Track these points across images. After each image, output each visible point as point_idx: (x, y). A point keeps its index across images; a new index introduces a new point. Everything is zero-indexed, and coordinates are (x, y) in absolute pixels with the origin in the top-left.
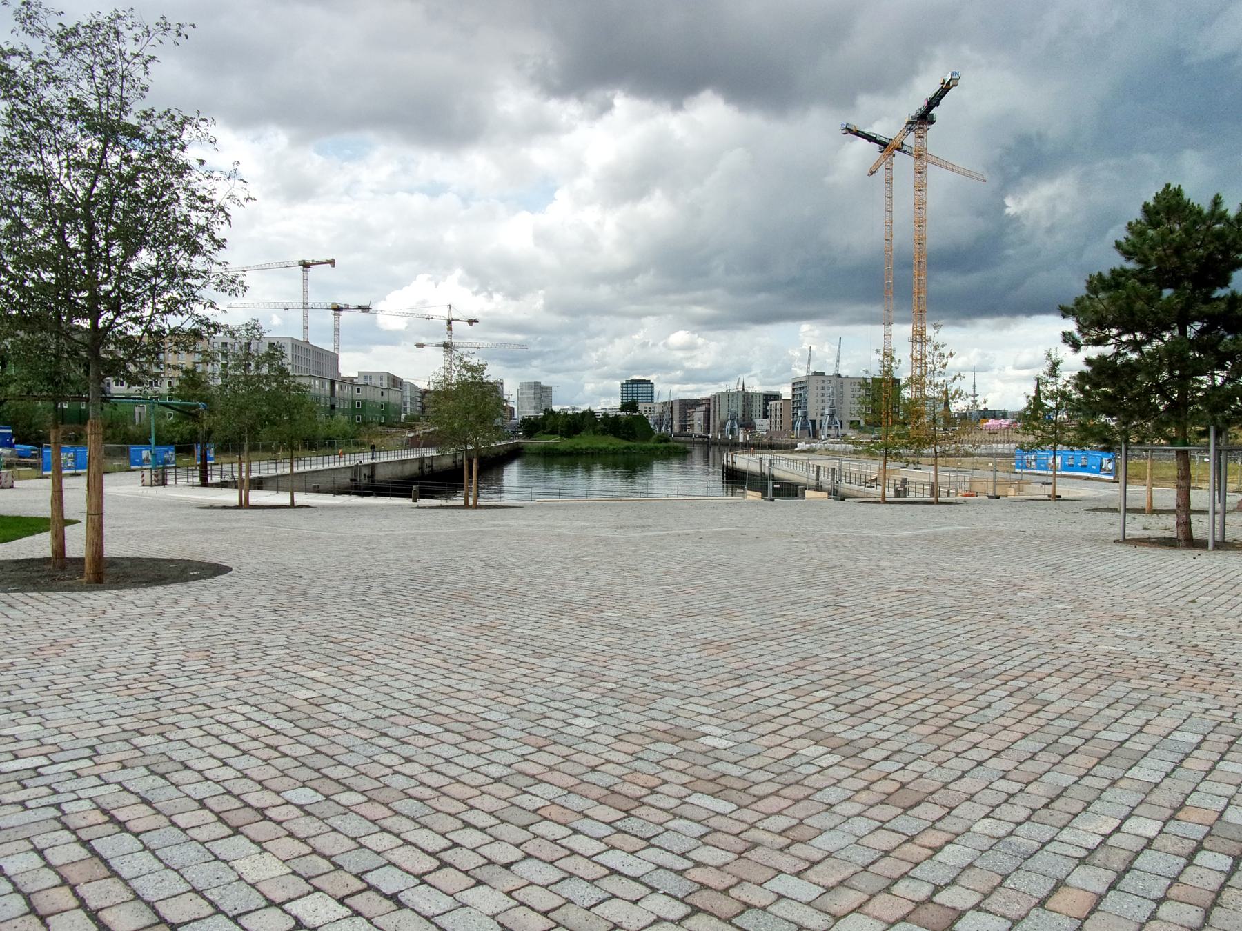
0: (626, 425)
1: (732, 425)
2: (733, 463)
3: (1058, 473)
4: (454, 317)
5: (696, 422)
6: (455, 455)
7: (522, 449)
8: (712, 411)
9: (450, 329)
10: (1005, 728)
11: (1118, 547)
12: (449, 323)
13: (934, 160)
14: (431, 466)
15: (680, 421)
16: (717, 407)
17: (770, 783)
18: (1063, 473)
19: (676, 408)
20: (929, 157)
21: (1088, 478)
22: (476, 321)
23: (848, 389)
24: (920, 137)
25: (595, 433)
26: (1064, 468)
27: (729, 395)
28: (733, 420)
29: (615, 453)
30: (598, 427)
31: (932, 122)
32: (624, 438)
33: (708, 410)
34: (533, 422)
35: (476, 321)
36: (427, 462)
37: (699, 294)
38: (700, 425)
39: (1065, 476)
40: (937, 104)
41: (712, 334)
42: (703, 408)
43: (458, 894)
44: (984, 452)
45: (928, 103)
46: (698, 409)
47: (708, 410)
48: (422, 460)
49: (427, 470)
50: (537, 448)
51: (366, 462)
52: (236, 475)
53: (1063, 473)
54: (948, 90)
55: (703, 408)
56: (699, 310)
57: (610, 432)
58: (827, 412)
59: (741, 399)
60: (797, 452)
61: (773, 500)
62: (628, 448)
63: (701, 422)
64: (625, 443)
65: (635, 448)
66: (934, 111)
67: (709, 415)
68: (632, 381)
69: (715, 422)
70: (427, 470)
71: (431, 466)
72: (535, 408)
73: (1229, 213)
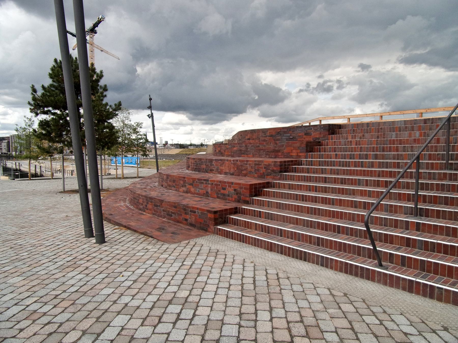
2: (6, 165)
3: (124, 165)
5: (3, 147)
8: (11, 142)
10: (118, 254)
11: (63, 195)
13: (97, 46)
17: (4, 294)
18: (126, 165)
20: (95, 45)
21: (133, 167)
24: (91, 38)
26: (128, 163)
31: (96, 33)
33: (9, 142)
37: (7, 91)
38: (5, 148)
39: (126, 166)
40: (97, 26)
41: (13, 109)
42: (6, 141)
43: (340, 330)
45: (94, 25)
46: (4, 141)
47: (9, 142)
52: (103, 157)
53: (126, 165)
54: (101, 22)
55: (6, 141)
56: (6, 98)
61: (14, 179)
63: (6, 147)
66: (96, 29)
67: (9, 144)
73: (46, 85)
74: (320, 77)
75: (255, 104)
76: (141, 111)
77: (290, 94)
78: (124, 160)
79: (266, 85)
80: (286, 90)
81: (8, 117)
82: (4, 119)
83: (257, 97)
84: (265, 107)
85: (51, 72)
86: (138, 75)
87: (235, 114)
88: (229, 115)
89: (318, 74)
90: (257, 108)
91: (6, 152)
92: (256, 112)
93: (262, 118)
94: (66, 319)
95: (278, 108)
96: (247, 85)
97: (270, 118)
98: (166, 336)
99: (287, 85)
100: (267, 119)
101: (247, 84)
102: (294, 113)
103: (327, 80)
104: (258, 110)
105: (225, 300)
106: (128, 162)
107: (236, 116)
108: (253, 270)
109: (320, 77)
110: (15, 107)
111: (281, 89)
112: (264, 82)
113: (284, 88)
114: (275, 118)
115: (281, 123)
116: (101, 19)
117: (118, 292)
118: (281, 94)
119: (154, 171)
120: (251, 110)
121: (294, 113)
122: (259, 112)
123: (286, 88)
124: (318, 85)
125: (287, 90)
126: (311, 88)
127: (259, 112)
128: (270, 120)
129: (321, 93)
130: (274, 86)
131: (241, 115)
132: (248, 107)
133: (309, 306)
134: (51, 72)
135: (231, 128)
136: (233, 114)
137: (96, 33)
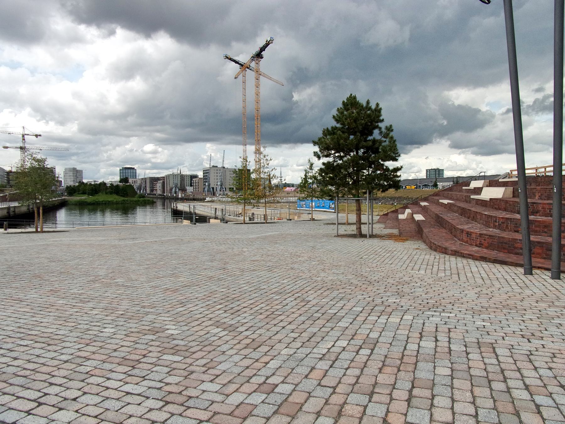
0: (122, 190)
1: (175, 190)
3: (313, 209)
4: (26, 133)
6: (29, 206)
7: (67, 202)
8: (165, 183)
9: (24, 139)
12: (23, 136)
14: (14, 211)
15: (150, 188)
16: (168, 181)
18: (316, 209)
19: (148, 181)
21: (325, 211)
22: (40, 136)
23: (228, 173)
25: (106, 193)
26: (318, 207)
27: (174, 175)
28: (176, 187)
29: (117, 203)
30: (108, 191)
31: (262, 58)
32: (121, 196)
33: (164, 182)
34: (73, 188)
35: (40, 136)
36: (12, 209)
37: (159, 127)
39: (316, 211)
40: (264, 50)
42: (161, 181)
44: (285, 201)
46: (159, 182)
47: (164, 182)
48: (9, 208)
49: (12, 213)
50: (75, 201)
51: (12, 206)
53: (316, 209)
54: (269, 44)
56: (158, 135)
57: (115, 193)
58: (219, 184)
59: (179, 177)
60: (206, 202)
62: (124, 200)
63: (161, 188)
64: (122, 198)
65: (127, 201)
66: (263, 53)
67: (164, 185)
68: (125, 168)
69: (167, 188)
70: (12, 213)
71: (14, 211)
72: (74, 181)
74: (539, 90)
75: (443, 132)
76: (300, 145)
77: (493, 116)
78: (313, 204)
79: (460, 107)
80: (487, 111)
81: (157, 155)
82: (155, 157)
83: (445, 123)
84: (458, 135)
85: (330, 129)
86: (297, 102)
87: (417, 146)
88: (409, 146)
89: (536, 86)
90: (446, 137)
91: (161, 193)
92: (445, 143)
93: (453, 150)
94: (201, 357)
95: (477, 136)
96: (433, 107)
97: (464, 150)
98: (294, 386)
99: (488, 104)
100: (460, 151)
101: (433, 106)
102: (499, 142)
103: (550, 95)
104: (448, 139)
105: (434, 354)
106: (319, 206)
107: (418, 148)
108: (438, 328)
109: (539, 90)
110: (165, 145)
111: (480, 111)
112: (457, 103)
113: (484, 108)
114: (472, 149)
115: (480, 155)
116: (269, 42)
117: (349, 334)
118: (480, 116)
119: (339, 215)
120: (438, 140)
121: (499, 142)
122: (449, 142)
123: (488, 108)
124: (535, 102)
125: (489, 112)
126: (524, 107)
127: (449, 142)
128: (463, 153)
129: (540, 113)
130: (470, 107)
131: (424, 146)
132: (435, 135)
133: (486, 376)
134: (330, 129)
135: (411, 163)
136: (415, 146)
137: (262, 58)
